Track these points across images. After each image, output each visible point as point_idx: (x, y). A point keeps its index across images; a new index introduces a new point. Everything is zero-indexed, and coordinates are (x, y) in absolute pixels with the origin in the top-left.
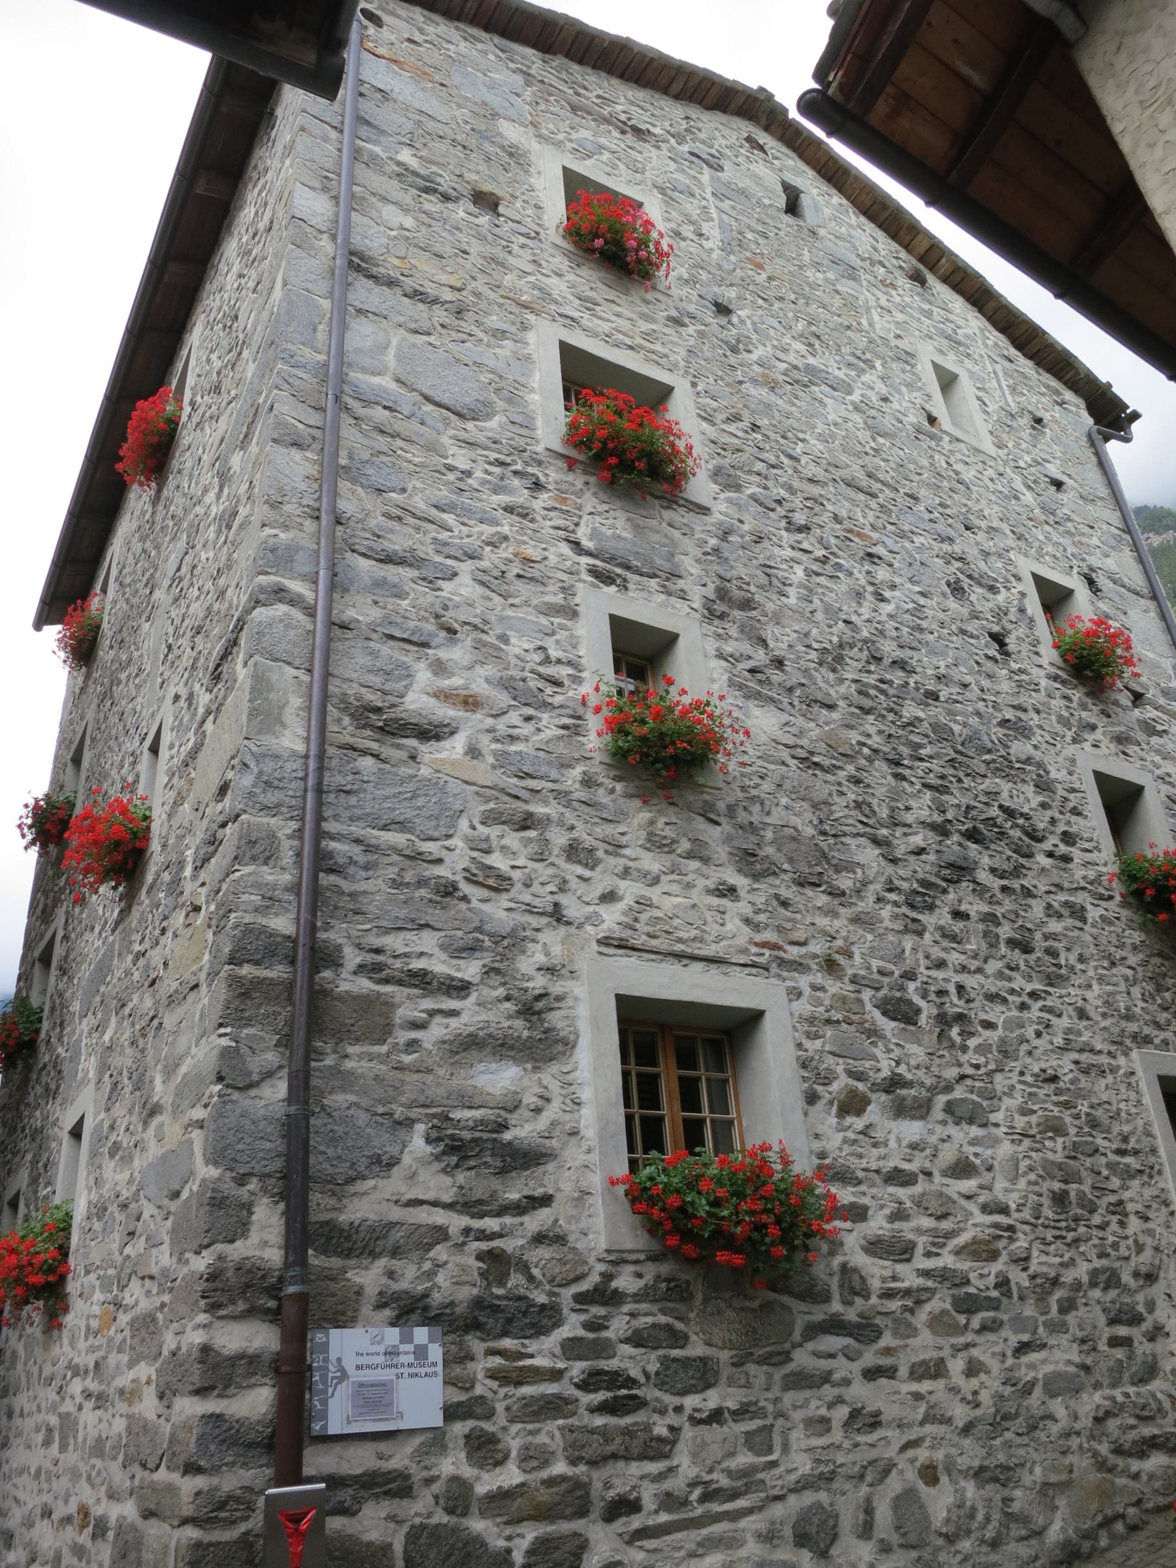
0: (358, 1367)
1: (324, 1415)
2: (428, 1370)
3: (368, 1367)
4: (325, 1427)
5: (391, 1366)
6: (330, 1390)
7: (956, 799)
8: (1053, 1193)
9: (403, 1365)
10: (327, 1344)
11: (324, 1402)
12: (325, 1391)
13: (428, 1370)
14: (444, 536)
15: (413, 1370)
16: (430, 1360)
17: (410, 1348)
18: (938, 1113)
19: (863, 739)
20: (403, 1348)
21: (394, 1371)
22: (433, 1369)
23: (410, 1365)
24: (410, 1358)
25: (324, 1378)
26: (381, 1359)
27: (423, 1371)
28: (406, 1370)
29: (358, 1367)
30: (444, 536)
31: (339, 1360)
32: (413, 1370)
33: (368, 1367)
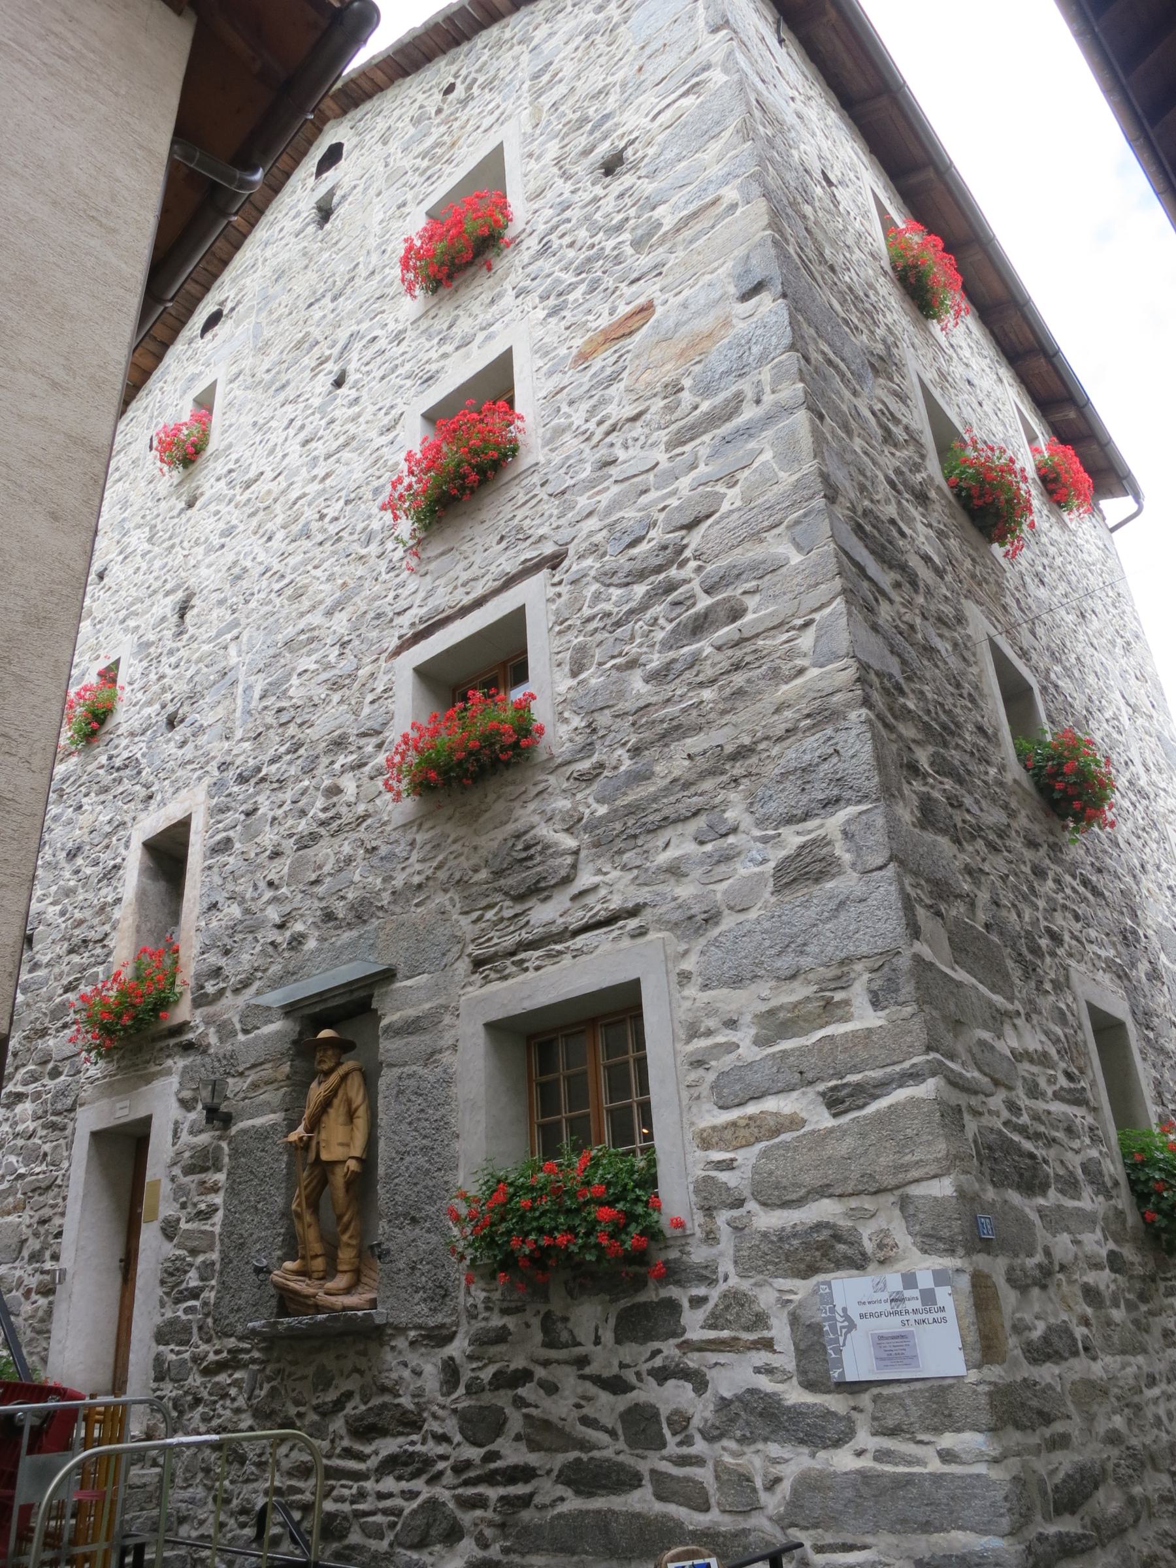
0: (862, 1316)
1: (839, 1363)
2: (935, 1315)
3: (871, 1315)
4: (842, 1374)
5: (896, 1313)
6: (841, 1339)
7: (982, 769)
8: (956, 1036)
9: (907, 1312)
10: (831, 1294)
11: (839, 1351)
12: (836, 1341)
13: (935, 1315)
14: (450, 840)
15: (918, 1317)
16: (940, 1304)
17: (915, 1293)
18: (289, 845)
19: (192, 522)
20: (908, 1293)
21: (899, 1318)
22: (940, 1315)
23: (915, 1311)
24: (918, 1304)
25: (833, 1328)
26: (887, 1307)
27: (930, 1317)
28: (912, 1317)
29: (862, 1316)
30: (450, 840)
31: (845, 1310)
32: (918, 1317)
33: (871, 1315)
